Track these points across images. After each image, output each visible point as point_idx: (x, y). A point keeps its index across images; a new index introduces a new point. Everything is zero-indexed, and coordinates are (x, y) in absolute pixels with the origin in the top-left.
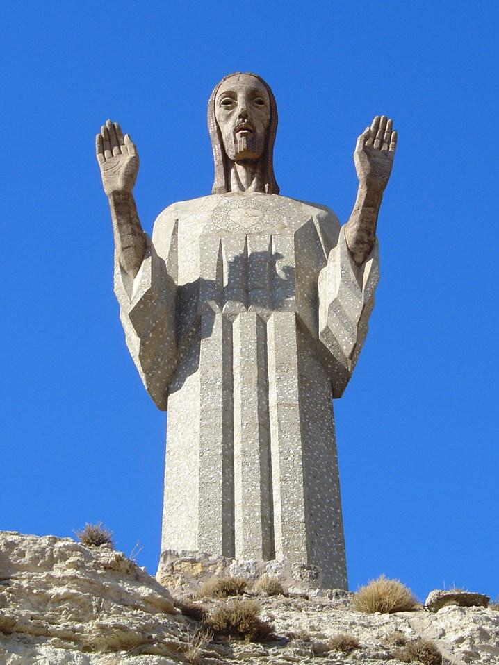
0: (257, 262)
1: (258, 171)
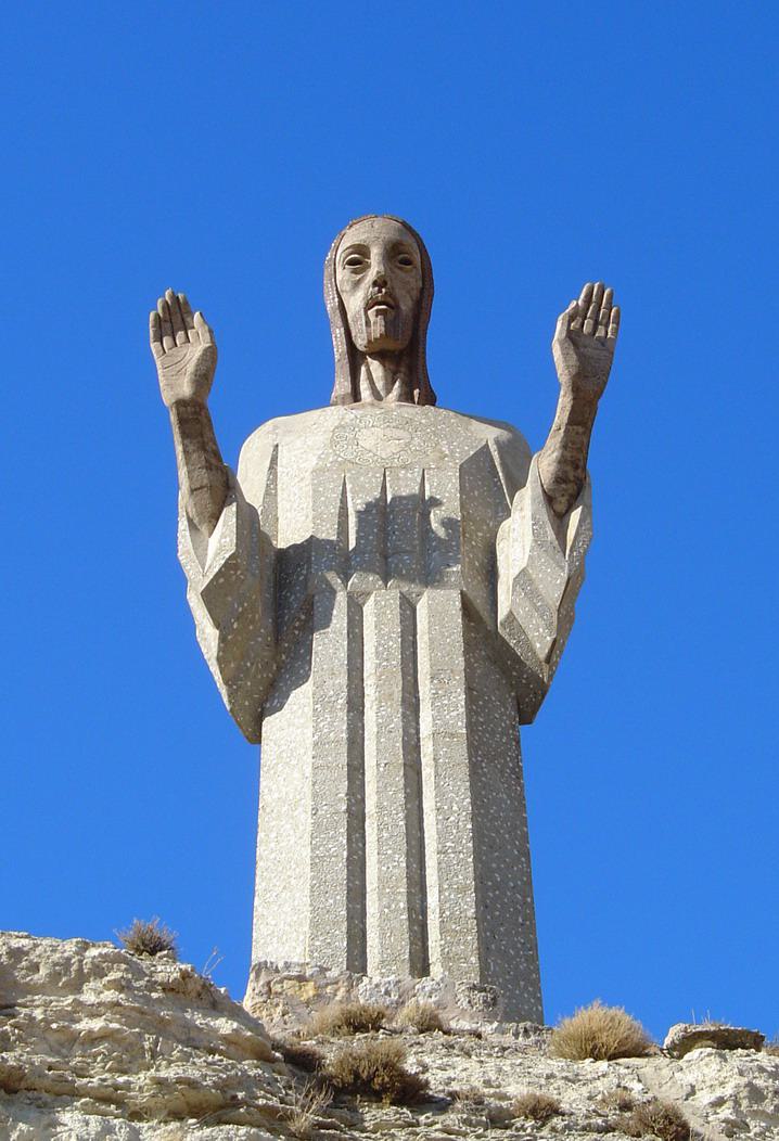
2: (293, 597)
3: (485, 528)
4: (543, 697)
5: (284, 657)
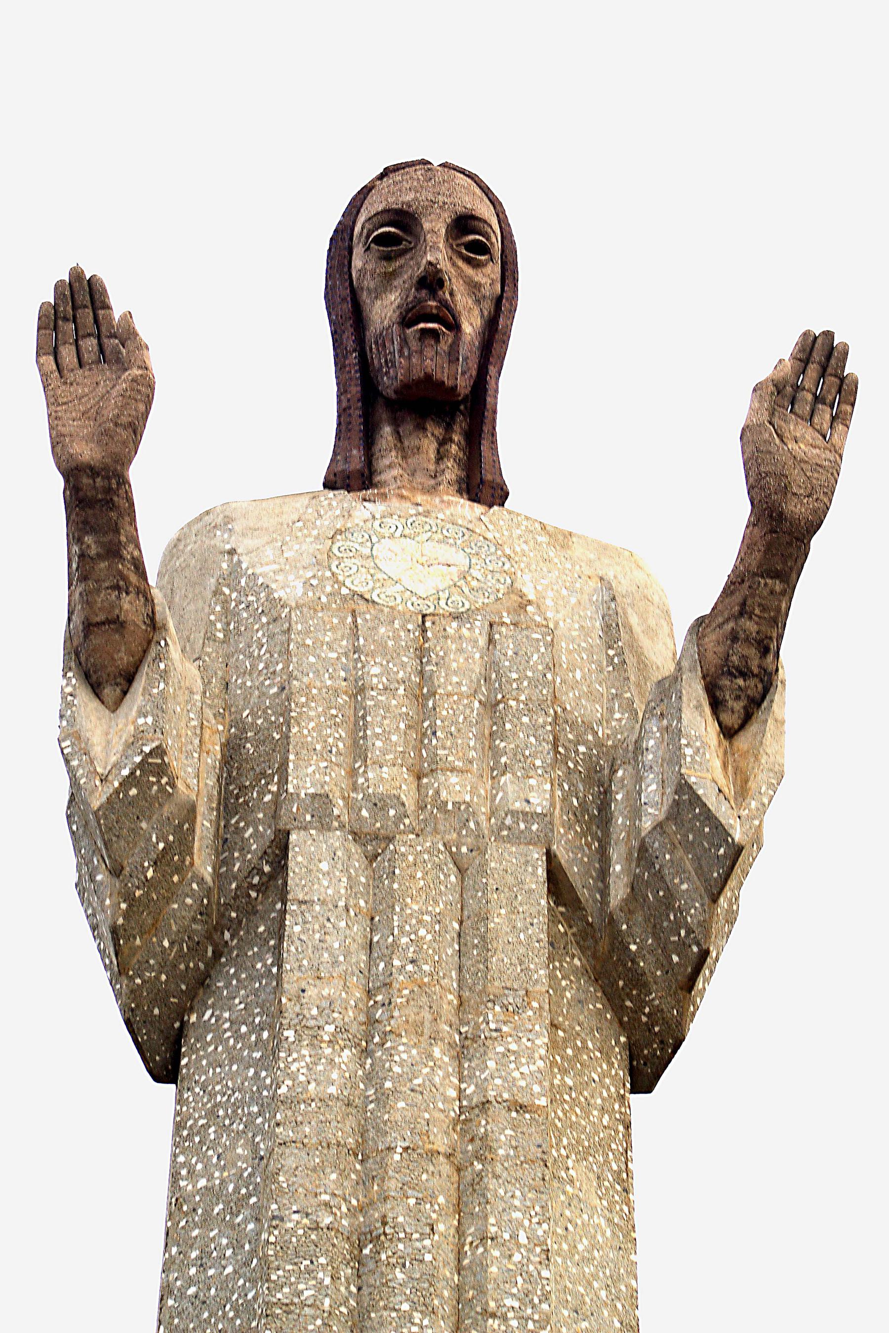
0: (449, 695)
1: (456, 438)
2: (251, 830)
3: (590, 737)
4: (674, 1052)
5: (227, 935)
